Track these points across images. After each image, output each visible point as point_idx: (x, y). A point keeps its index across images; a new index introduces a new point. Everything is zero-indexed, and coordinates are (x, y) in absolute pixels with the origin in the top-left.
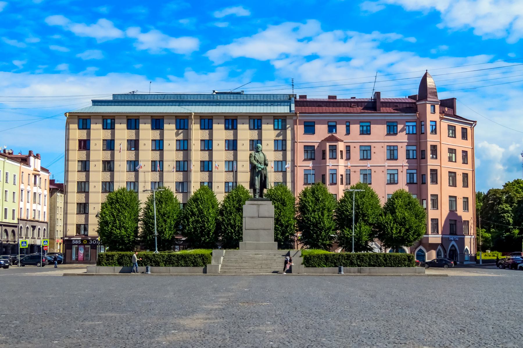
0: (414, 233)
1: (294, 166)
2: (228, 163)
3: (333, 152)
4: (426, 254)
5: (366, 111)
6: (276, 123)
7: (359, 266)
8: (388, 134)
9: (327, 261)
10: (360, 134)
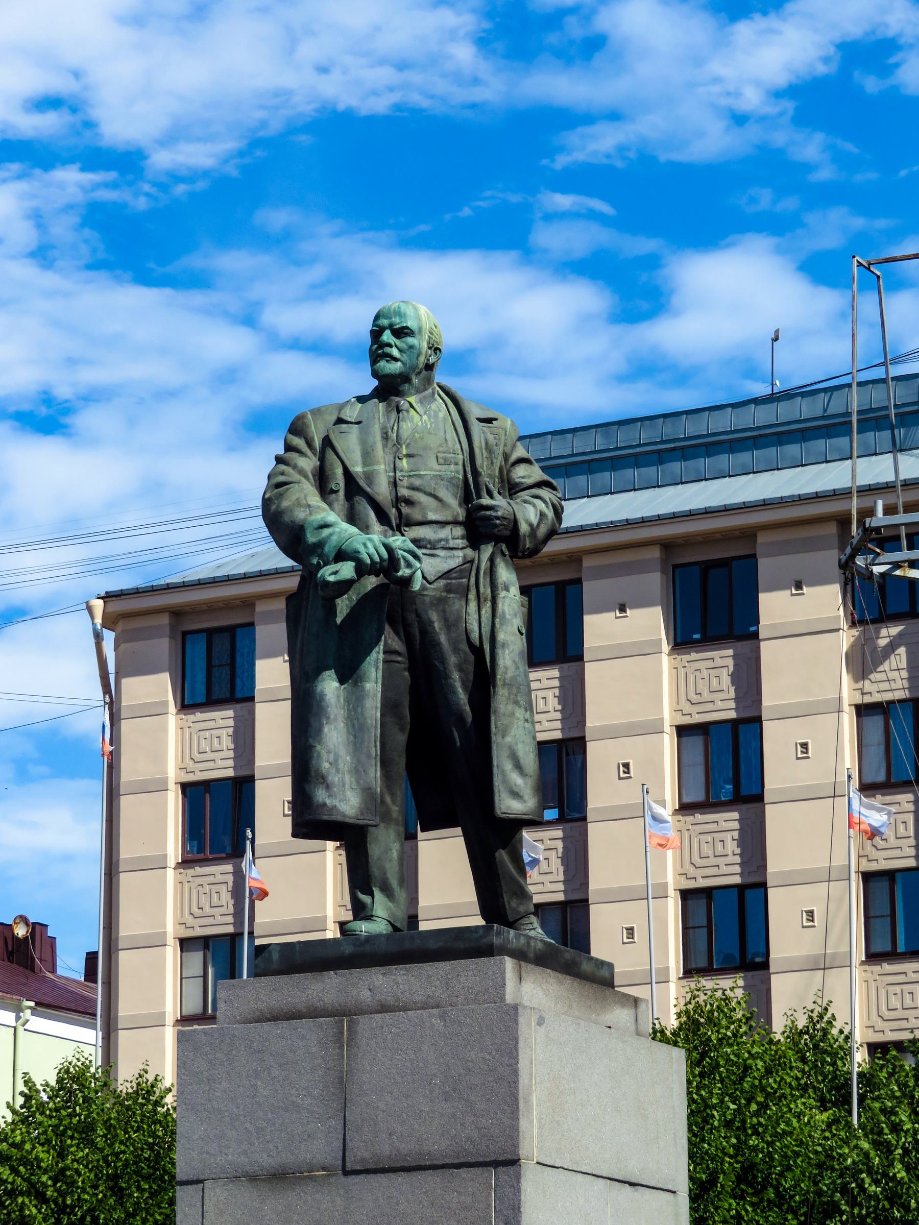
2: (884, 885)
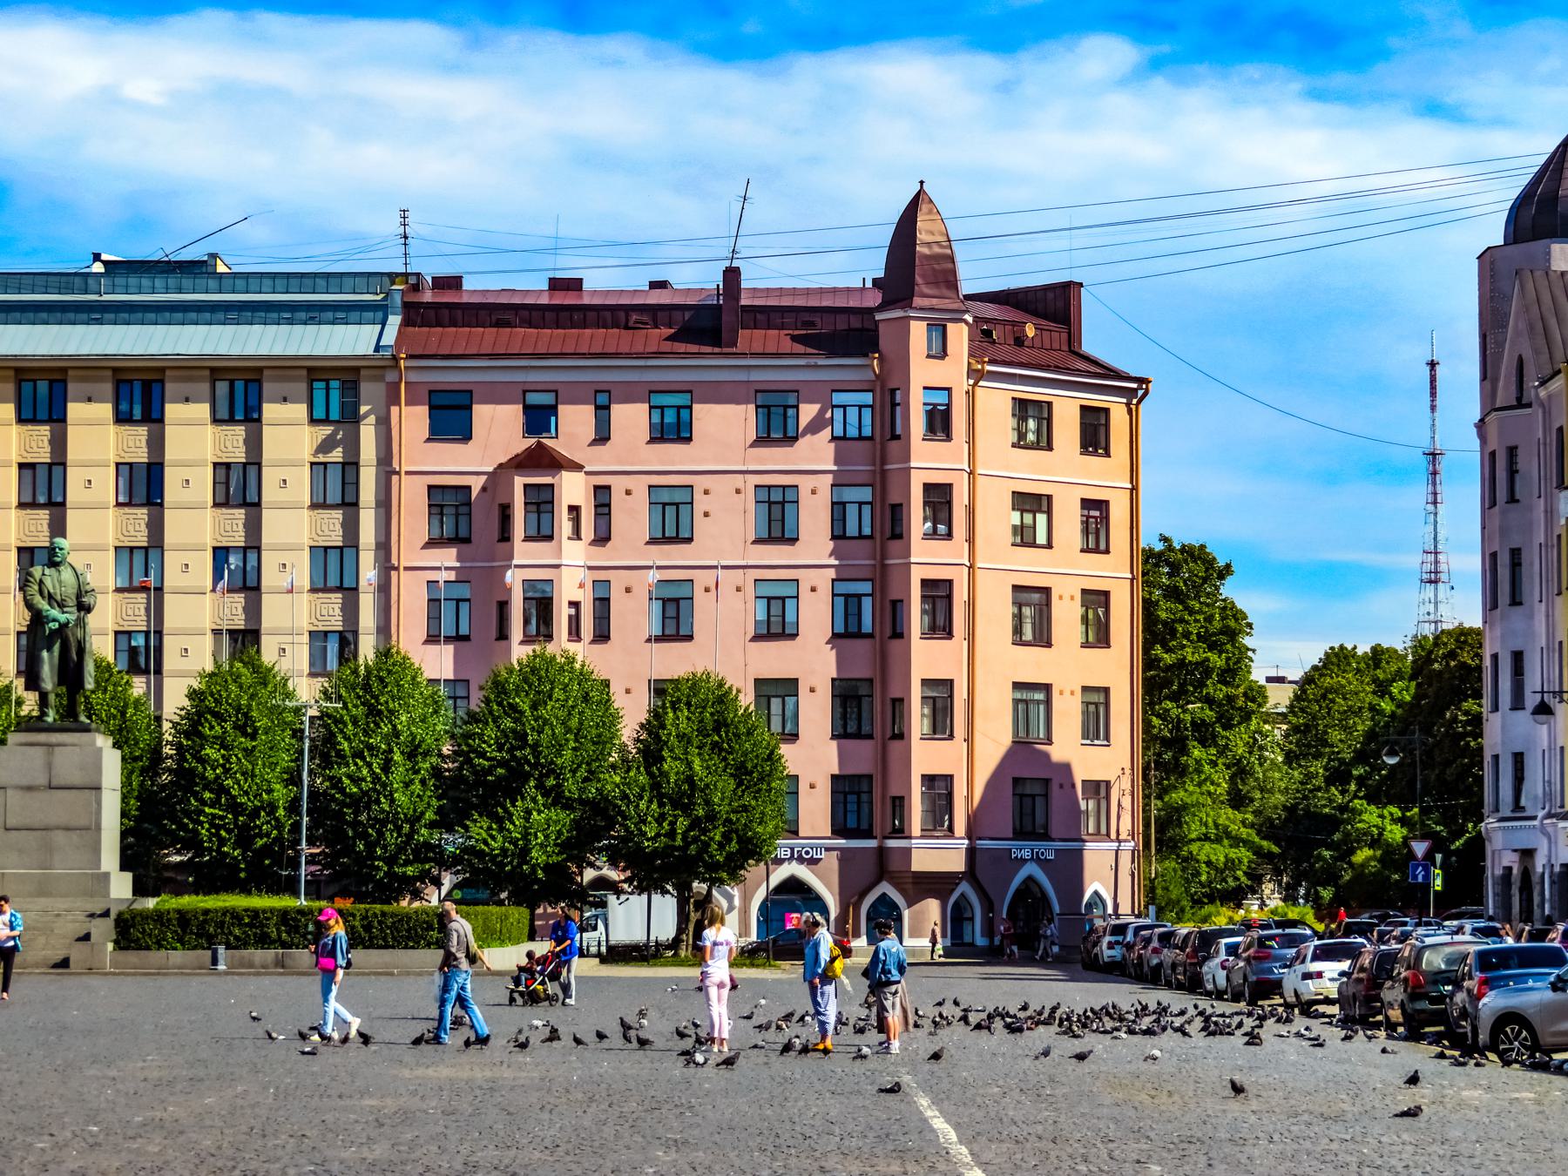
0: (727, 837)
1: (387, 567)
2: (126, 554)
3: (539, 513)
4: (906, 914)
5: (694, 348)
6: (319, 396)
7: (285, 945)
8: (763, 440)
9: (184, 931)
10: (652, 440)
